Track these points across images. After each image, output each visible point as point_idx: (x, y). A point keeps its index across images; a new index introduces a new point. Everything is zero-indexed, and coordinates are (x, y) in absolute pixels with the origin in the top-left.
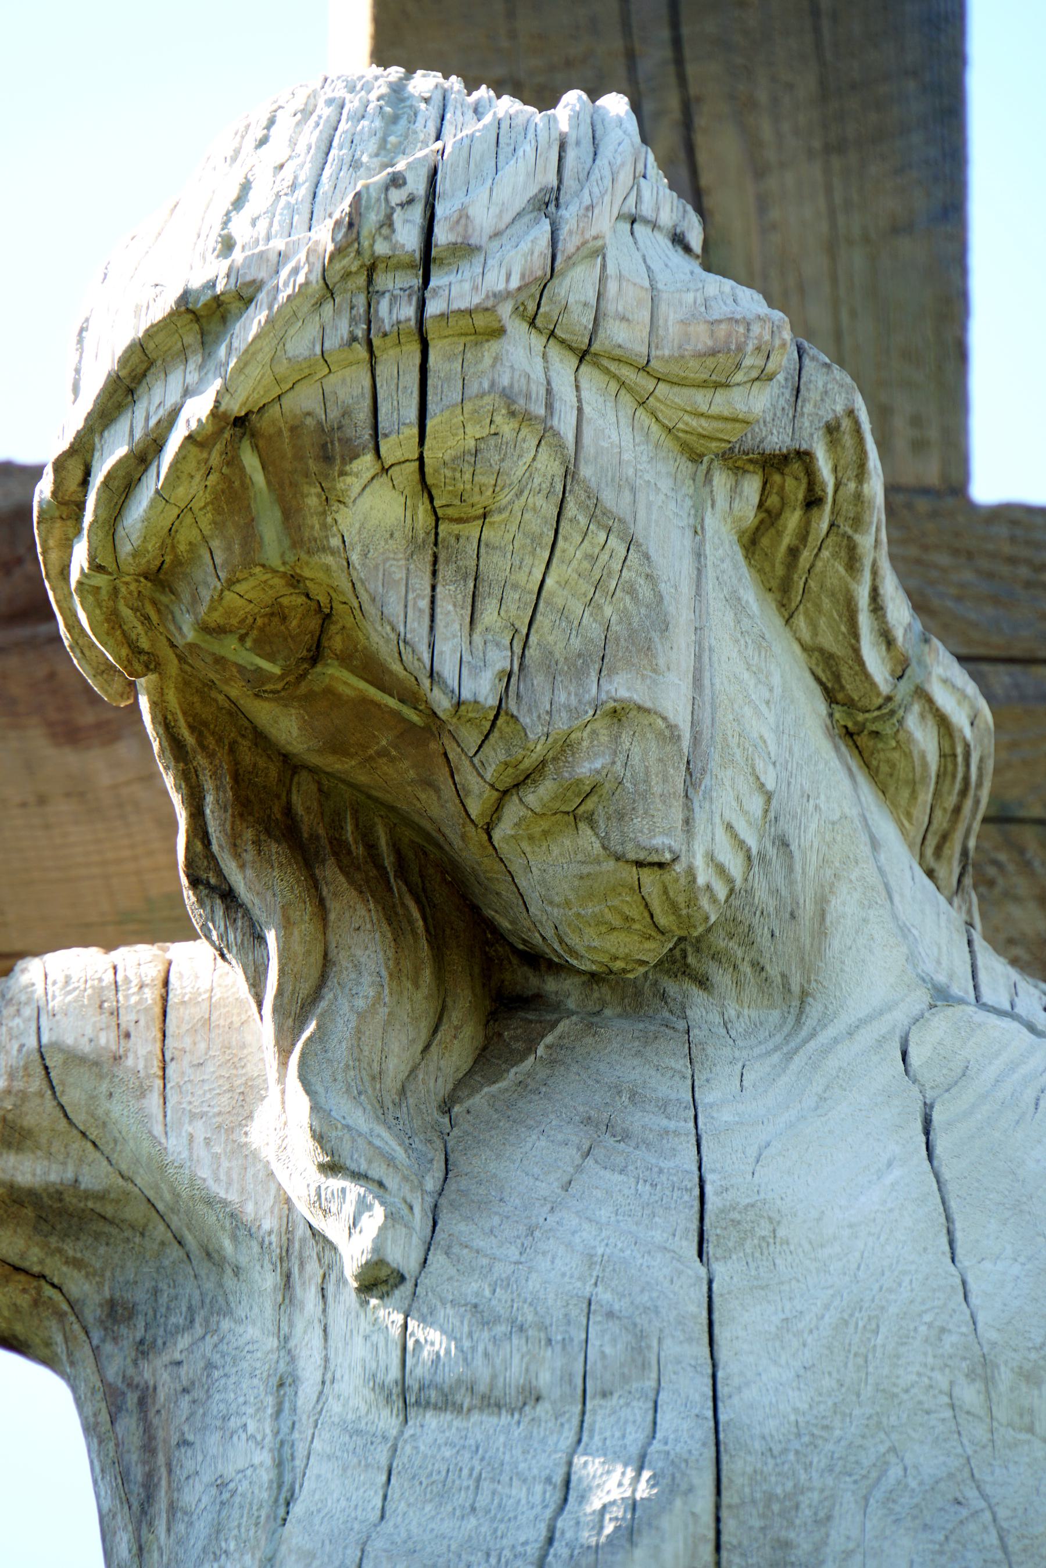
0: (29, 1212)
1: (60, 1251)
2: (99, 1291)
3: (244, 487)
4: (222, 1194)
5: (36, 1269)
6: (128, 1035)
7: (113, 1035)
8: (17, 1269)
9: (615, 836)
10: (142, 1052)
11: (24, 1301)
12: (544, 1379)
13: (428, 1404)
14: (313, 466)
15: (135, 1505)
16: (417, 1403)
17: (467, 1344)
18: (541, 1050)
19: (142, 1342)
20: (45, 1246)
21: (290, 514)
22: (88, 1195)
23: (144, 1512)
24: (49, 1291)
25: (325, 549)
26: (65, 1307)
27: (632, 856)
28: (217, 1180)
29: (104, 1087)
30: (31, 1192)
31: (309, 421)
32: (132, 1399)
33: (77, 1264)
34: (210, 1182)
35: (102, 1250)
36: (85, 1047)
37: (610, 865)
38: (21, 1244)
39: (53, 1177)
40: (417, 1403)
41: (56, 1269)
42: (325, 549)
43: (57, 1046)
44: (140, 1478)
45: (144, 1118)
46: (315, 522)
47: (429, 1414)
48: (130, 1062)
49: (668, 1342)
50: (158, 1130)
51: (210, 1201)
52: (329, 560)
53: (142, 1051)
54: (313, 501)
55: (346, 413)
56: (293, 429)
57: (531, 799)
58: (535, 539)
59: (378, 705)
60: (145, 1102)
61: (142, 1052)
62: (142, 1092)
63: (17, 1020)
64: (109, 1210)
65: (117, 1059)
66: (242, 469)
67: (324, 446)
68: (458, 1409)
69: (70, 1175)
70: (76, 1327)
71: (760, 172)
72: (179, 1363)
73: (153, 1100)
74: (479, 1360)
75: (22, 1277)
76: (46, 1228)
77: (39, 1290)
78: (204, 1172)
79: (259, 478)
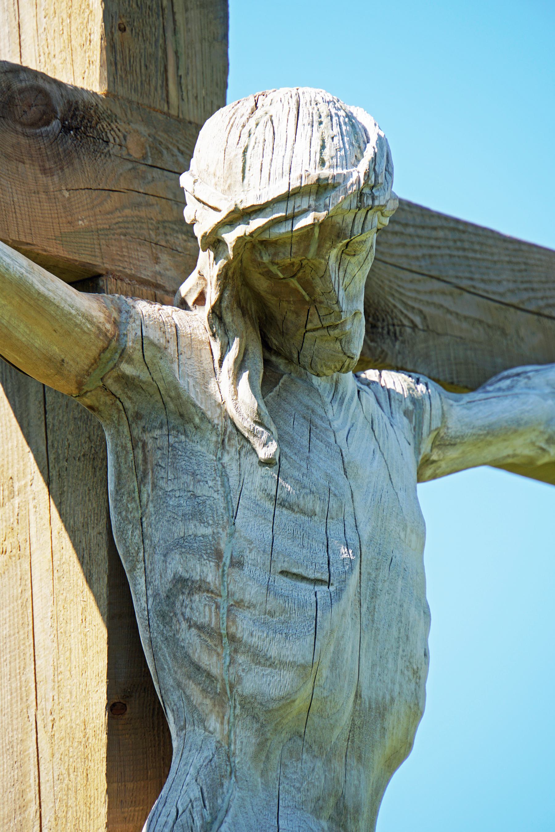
0: (124, 381)
1: (126, 393)
2: (134, 408)
3: (312, 236)
4: (199, 405)
5: (118, 396)
6: (168, 342)
7: (164, 340)
8: (113, 394)
9: (346, 348)
10: (172, 349)
11: (109, 402)
12: (317, 510)
13: (284, 506)
14: (333, 237)
15: (139, 478)
16: (280, 504)
17: (298, 492)
18: (280, 384)
19: (144, 427)
20: (123, 390)
21: (320, 247)
22: (141, 381)
23: (142, 480)
24: (118, 402)
25: (324, 258)
26: (121, 408)
27: (349, 355)
28: (197, 399)
29: (159, 355)
30: (128, 377)
31: (338, 225)
32: (140, 444)
33: (130, 398)
34: (195, 400)
35: (137, 396)
36: (156, 342)
37: (341, 355)
38: (117, 388)
39: (134, 374)
40: (280, 504)
41: (123, 398)
42: (324, 258)
43: (147, 337)
44: (141, 470)
45: (172, 371)
46: (325, 251)
47: (284, 509)
48: (169, 351)
49: (346, 506)
50: (177, 376)
51: (195, 405)
52: (323, 261)
53: (172, 348)
54: (328, 246)
55: (347, 226)
56: (332, 226)
57: (331, 332)
58: (360, 263)
59: (299, 292)
60: (173, 366)
61: (172, 349)
62: (172, 362)
63: (134, 324)
64: (144, 387)
65: (166, 348)
66: (314, 231)
67: (339, 233)
68: (293, 510)
69: (138, 374)
70: (124, 415)
71: (187, 10)
72: (156, 439)
73: (175, 366)
74: (301, 499)
75: (113, 396)
76: (126, 386)
77: (115, 401)
78: (193, 395)
79: (317, 235)
